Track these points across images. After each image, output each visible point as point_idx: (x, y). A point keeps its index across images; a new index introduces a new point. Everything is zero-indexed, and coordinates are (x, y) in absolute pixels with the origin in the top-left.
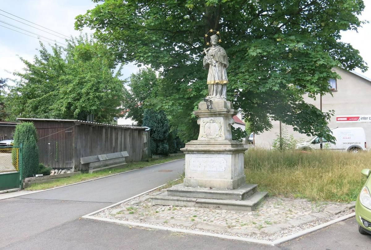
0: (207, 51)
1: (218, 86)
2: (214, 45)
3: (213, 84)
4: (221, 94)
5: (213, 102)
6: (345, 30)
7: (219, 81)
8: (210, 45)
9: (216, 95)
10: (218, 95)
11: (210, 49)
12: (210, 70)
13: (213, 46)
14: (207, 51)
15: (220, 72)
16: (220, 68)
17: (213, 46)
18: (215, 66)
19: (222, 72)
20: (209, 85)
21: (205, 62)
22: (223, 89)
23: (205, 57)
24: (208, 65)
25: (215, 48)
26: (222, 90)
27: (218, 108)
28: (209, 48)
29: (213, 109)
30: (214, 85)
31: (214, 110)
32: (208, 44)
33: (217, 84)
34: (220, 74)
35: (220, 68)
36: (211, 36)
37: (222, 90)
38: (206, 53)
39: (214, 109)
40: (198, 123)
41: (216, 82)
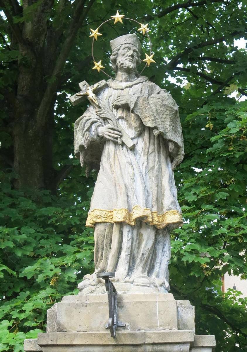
0: (97, 92)
1: (139, 235)
2: (128, 71)
3: (121, 224)
4: (150, 269)
5: (125, 301)
6: (172, 77)
7: (148, 213)
8: (108, 74)
9: (131, 269)
10: (138, 272)
11: (107, 86)
12: (104, 162)
13: (121, 75)
14: (97, 92)
15: (152, 175)
16: (151, 157)
17: (121, 75)
18: (133, 149)
19: (159, 176)
20: (99, 230)
21: (89, 130)
22: (160, 247)
23: (91, 114)
24: (96, 148)
25: (129, 84)
26: (153, 252)
27: (150, 328)
28: (103, 82)
29: (123, 331)
30: (126, 230)
31: (133, 335)
32: (98, 66)
33: (141, 223)
34: (152, 184)
35: (154, 158)
36: (114, 38)
37: (153, 252)
38: (91, 95)
39: (129, 331)
40: (148, 351)
41: (136, 214)
